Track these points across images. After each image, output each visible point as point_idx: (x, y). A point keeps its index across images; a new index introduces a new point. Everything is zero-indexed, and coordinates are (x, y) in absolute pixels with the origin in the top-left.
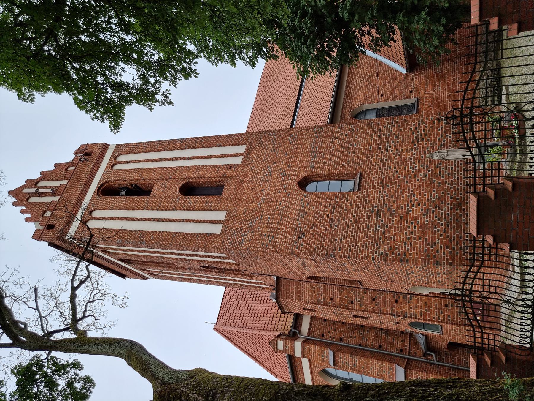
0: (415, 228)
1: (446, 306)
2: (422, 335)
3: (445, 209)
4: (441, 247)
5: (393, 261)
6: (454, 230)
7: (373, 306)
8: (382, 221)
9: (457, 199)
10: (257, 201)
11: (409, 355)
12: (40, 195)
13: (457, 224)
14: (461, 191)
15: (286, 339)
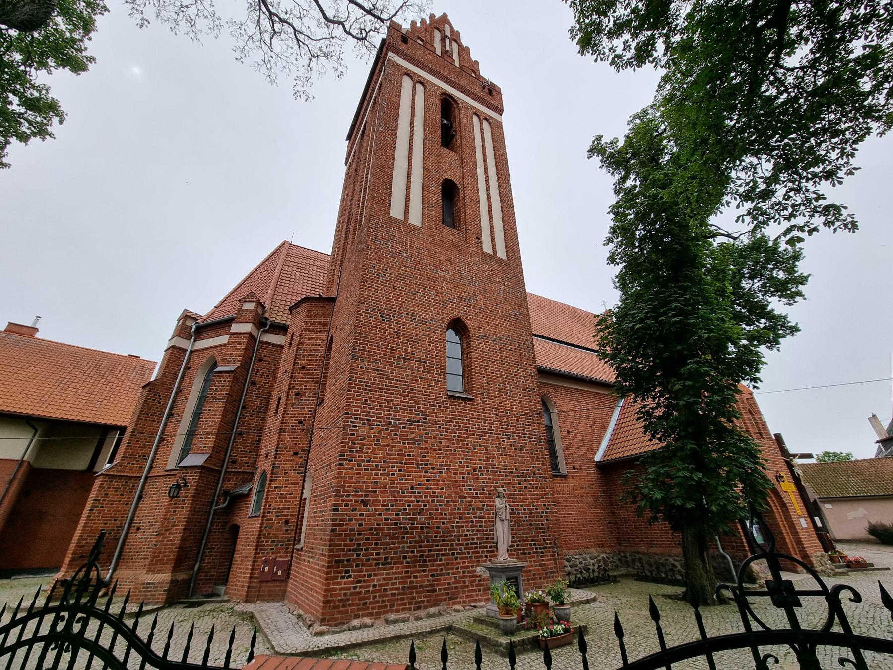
0: (393, 475)
1: (287, 522)
2: (250, 490)
3: (421, 518)
4: (362, 515)
5: (342, 442)
6: (389, 534)
7: (291, 422)
8: (404, 428)
9: (436, 536)
10: (435, 266)
11: (226, 472)
12: (443, 40)
13: (398, 538)
14: (448, 541)
15: (257, 312)
